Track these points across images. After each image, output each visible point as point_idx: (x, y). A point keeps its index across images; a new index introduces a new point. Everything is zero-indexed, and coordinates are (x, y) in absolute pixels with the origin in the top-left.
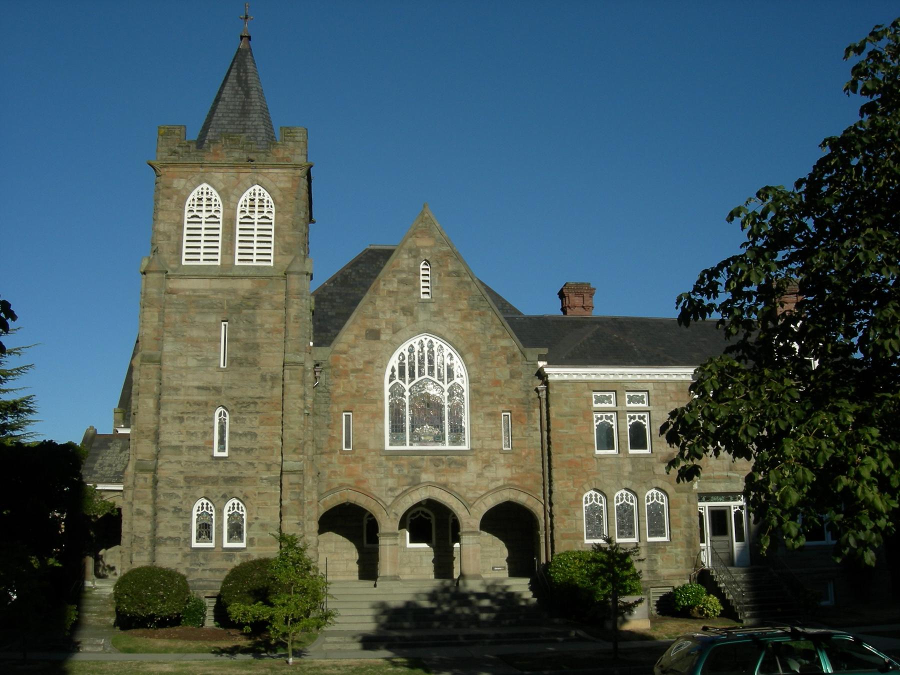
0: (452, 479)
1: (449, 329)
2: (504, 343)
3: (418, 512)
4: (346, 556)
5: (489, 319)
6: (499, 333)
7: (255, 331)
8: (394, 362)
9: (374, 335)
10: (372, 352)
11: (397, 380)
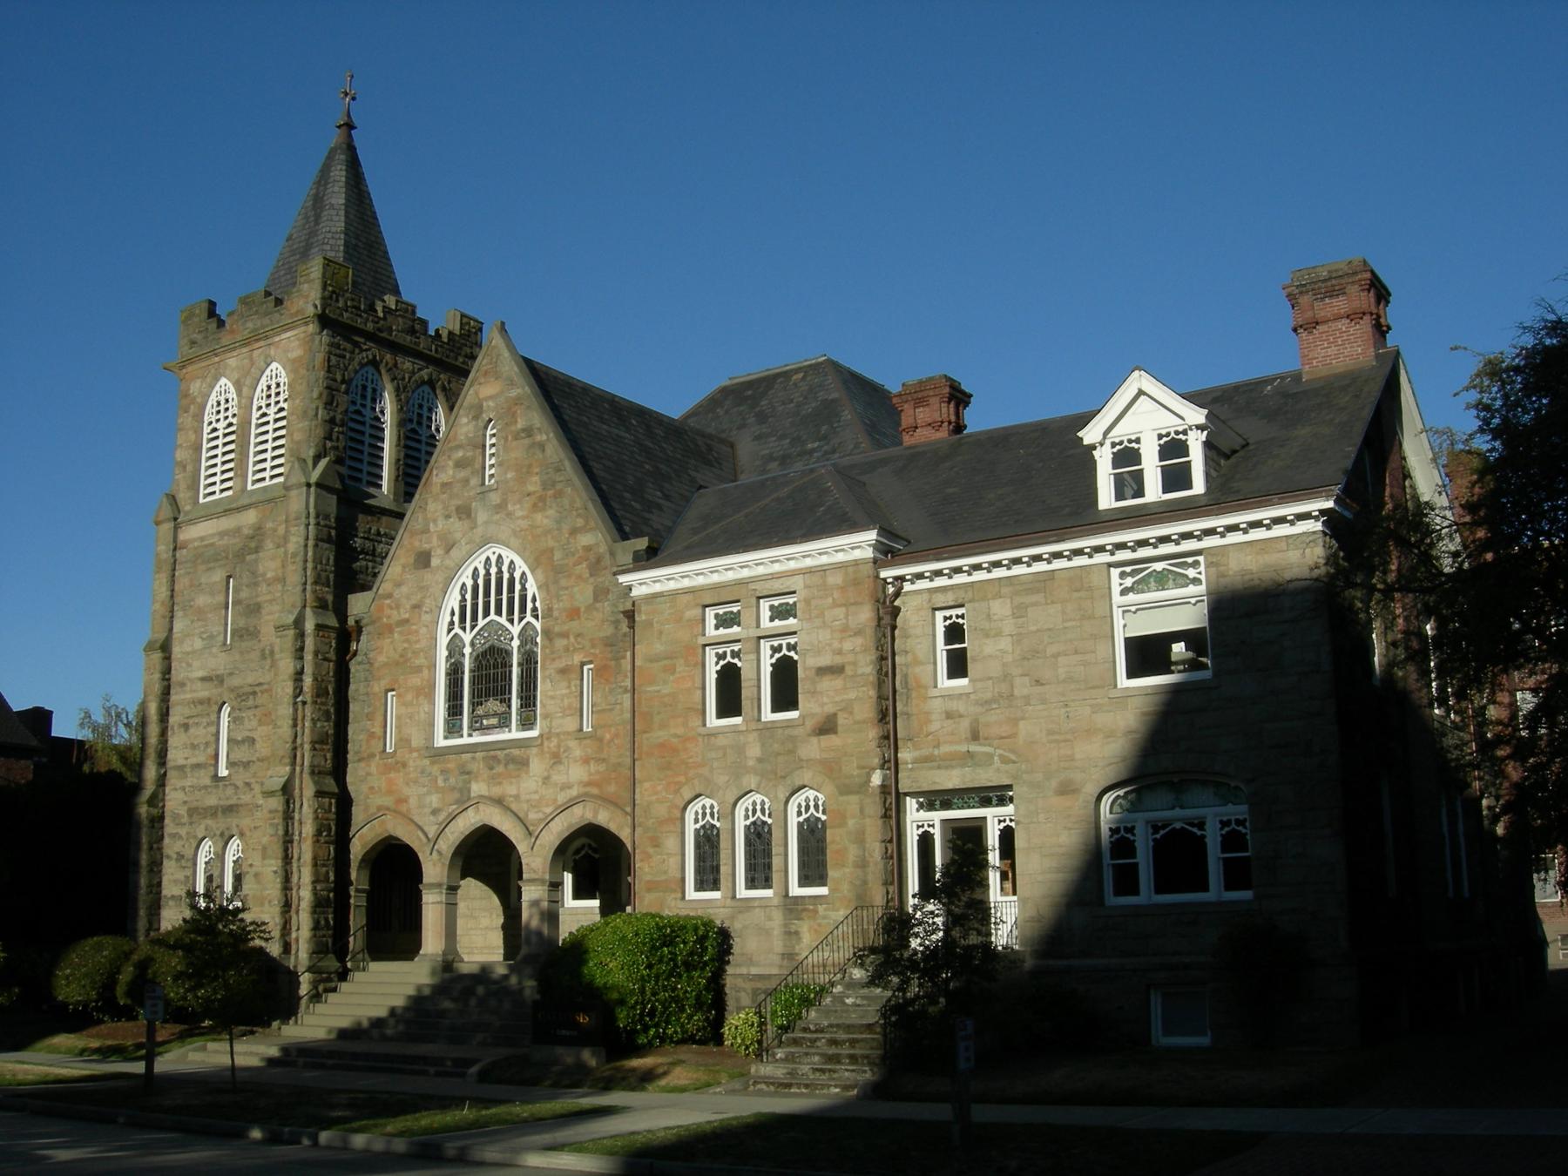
0: (510, 789)
1: (514, 532)
2: (586, 539)
3: (583, 846)
4: (485, 922)
5: (566, 501)
6: (580, 522)
7: (256, 584)
8: (453, 600)
9: (423, 560)
10: (421, 588)
11: (457, 630)
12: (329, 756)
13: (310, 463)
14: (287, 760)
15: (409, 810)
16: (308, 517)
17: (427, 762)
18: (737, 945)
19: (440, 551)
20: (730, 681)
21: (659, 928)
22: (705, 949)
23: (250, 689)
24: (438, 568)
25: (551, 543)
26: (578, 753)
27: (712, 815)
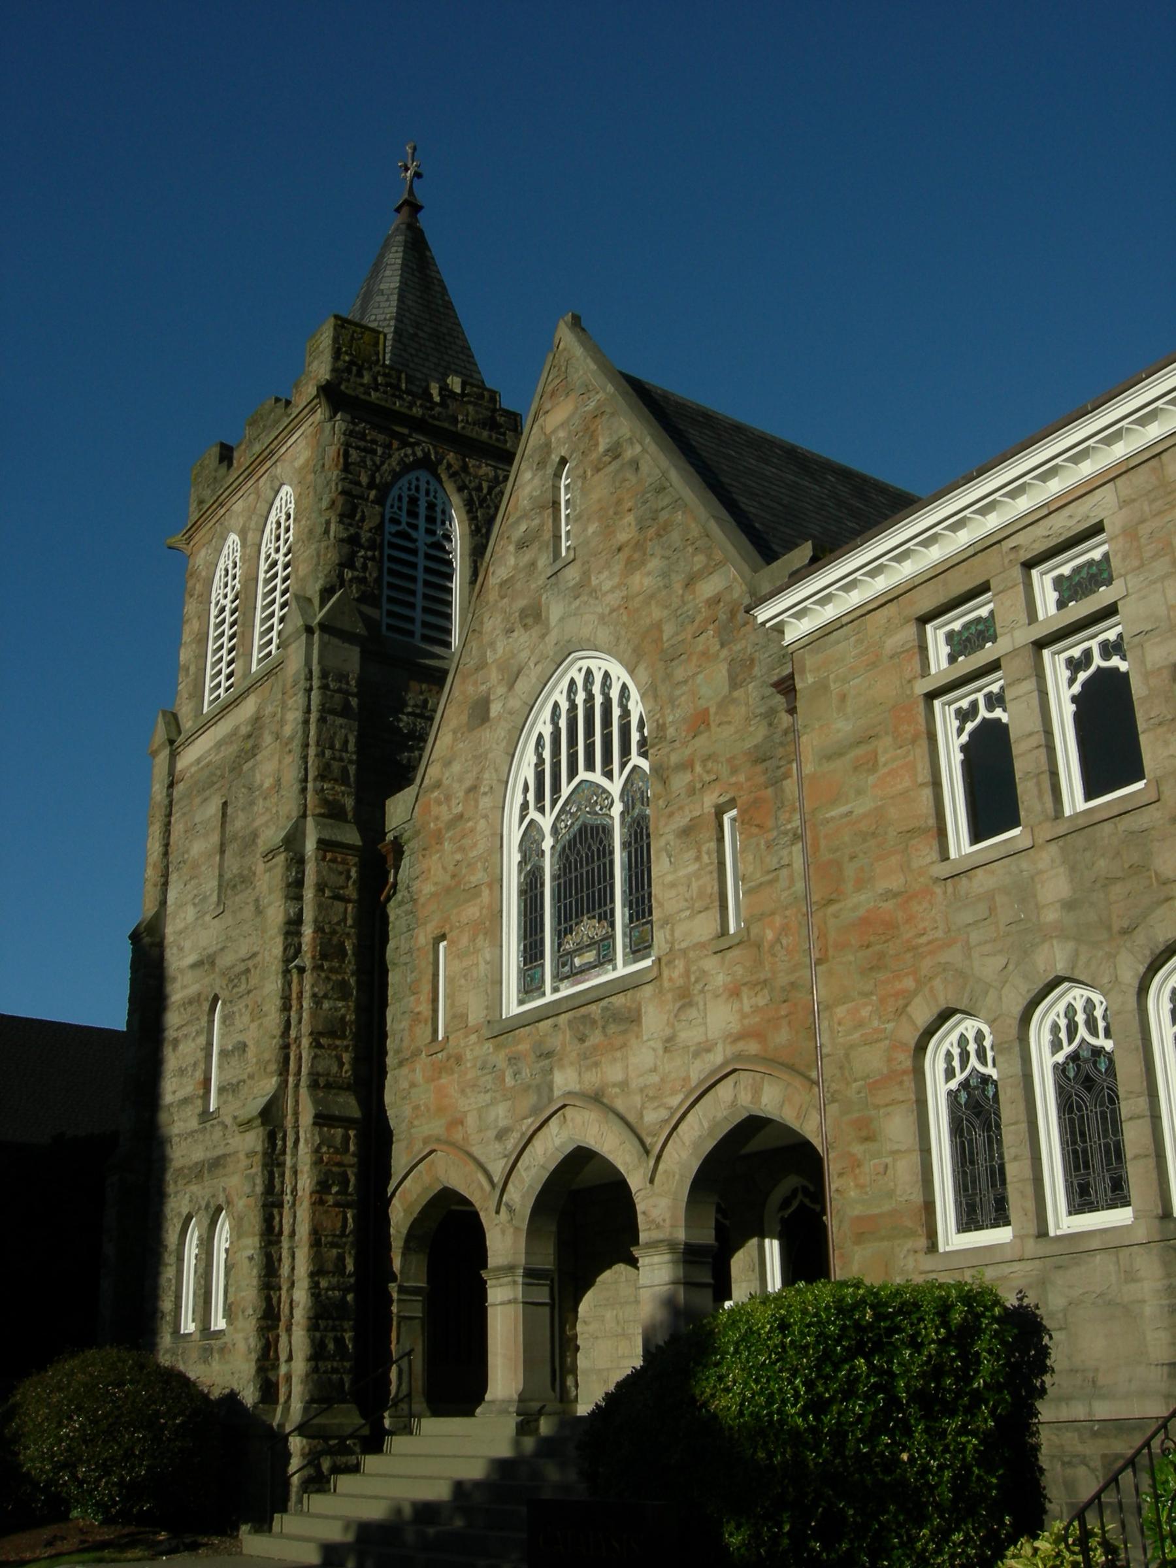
2: (709, 588)
3: (794, 1193)
8: (525, 770)
11: (533, 814)
12: (346, 1057)
13: (316, 601)
14: (273, 1067)
15: (466, 1139)
16: (309, 678)
17: (489, 1046)
18: (1061, 1351)
19: (501, 690)
20: (989, 757)
21: (843, 1310)
22: (971, 1361)
23: (241, 967)
24: (500, 717)
25: (657, 613)
26: (720, 979)
27: (981, 1055)
